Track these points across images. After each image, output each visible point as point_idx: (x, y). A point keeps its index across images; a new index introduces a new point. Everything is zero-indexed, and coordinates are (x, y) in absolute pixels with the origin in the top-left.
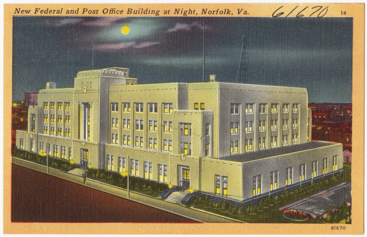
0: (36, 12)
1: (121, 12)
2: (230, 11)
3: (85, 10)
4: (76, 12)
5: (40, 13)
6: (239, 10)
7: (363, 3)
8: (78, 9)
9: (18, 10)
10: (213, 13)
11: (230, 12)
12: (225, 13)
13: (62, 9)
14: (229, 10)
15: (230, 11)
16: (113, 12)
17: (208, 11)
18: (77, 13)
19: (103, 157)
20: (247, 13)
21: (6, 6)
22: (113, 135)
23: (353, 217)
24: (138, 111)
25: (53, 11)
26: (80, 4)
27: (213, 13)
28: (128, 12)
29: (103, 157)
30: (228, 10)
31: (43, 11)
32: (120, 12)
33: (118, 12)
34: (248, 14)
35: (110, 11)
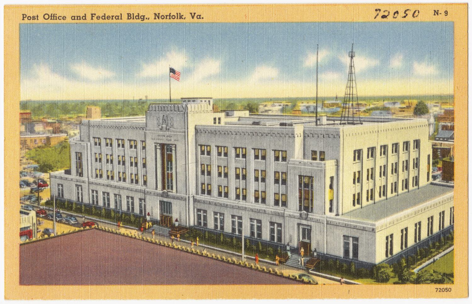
0: (92, 18)
1: (64, 18)
2: (182, 16)
3: (25, 16)
4: (84, 18)
5: (197, 19)
6: (191, 14)
7: (465, 4)
8: (85, 14)
9: (193, 14)
10: (166, 17)
11: (182, 17)
12: (177, 18)
13: (121, 14)
14: (181, 15)
15: (182, 16)
16: (55, 18)
17: (196, 15)
18: (85, 19)
19: (166, 207)
20: (201, 17)
21: (7, 7)
22: (108, 156)
23: (18, 110)
24: (279, 161)
25: (111, 17)
26: (184, 6)
27: (166, 17)
28: (128, 17)
29: (166, 207)
30: (180, 14)
31: (110, 17)
32: (62, 18)
33: (60, 18)
34: (203, 18)
35: (51, 16)
